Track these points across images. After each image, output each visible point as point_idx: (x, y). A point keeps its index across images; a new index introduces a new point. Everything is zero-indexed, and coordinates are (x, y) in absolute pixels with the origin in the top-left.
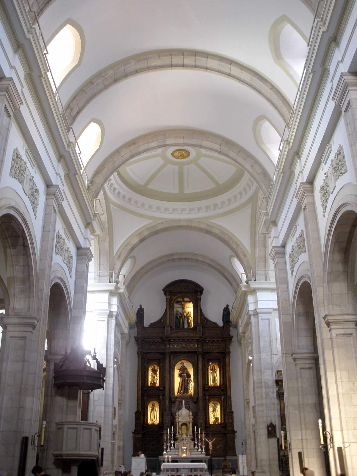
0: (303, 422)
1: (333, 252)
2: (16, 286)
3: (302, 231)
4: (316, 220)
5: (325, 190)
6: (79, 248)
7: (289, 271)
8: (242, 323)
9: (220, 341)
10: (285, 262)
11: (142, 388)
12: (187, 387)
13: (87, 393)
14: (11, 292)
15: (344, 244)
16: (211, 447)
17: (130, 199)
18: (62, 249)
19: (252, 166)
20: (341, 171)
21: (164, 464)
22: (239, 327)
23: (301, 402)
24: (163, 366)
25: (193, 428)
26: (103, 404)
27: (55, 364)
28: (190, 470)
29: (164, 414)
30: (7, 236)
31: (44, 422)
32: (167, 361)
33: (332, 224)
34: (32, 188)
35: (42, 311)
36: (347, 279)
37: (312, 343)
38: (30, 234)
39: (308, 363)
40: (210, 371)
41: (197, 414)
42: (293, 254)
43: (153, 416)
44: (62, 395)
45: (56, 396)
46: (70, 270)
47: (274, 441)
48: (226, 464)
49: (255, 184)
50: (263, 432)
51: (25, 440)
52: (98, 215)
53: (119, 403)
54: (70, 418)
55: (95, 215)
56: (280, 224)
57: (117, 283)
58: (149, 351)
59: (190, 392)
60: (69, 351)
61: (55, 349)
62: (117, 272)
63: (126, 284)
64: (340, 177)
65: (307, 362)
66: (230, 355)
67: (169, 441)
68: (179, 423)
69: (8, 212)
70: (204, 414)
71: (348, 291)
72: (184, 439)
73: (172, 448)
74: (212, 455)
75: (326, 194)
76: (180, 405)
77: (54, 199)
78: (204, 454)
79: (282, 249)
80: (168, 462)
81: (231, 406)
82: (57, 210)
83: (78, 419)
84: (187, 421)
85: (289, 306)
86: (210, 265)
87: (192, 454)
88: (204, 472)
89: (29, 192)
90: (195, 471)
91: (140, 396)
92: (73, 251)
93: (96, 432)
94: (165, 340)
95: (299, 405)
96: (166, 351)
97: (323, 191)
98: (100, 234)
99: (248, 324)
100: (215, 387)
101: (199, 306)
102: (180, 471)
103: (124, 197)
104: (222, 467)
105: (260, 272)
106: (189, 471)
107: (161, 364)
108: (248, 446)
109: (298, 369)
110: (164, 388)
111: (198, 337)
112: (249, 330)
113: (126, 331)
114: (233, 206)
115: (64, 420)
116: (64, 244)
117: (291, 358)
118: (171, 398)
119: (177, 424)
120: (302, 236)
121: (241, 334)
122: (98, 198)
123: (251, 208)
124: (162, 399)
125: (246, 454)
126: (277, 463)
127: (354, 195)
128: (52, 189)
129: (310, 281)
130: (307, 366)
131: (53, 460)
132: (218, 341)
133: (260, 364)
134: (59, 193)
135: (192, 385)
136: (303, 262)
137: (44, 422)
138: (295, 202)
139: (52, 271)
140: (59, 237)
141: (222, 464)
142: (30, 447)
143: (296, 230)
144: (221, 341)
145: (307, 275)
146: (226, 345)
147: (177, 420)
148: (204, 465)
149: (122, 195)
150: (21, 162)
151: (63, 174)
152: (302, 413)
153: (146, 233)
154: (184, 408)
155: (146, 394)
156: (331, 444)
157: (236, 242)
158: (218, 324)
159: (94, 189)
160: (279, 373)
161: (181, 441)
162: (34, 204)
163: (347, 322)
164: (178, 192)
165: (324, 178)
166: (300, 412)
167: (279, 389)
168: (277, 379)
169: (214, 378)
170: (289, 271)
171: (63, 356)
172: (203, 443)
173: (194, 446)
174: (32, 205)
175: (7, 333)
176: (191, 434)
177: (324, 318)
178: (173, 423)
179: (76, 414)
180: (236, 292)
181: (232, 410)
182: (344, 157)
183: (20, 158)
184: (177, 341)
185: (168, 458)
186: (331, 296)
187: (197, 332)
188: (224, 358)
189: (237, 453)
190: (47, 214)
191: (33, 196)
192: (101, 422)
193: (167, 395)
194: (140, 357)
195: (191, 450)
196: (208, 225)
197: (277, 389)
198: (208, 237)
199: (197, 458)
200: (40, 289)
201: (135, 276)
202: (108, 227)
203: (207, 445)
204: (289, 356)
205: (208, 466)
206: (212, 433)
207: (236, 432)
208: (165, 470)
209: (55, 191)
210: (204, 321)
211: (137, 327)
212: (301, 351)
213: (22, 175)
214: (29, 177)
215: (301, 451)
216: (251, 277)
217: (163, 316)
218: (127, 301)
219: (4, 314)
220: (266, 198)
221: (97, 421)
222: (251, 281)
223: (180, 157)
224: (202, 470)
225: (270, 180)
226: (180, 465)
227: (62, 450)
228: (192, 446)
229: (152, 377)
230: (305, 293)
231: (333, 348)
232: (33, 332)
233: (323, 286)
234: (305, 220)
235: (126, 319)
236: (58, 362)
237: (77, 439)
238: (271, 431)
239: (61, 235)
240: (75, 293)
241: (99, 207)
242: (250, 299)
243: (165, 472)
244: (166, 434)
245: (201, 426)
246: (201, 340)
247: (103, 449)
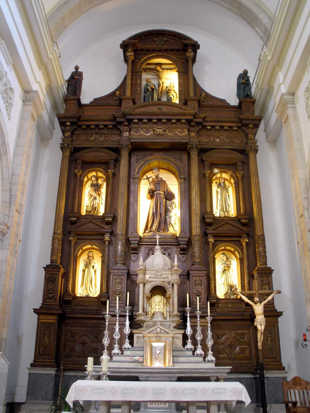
11: (66, 218)
12: (166, 219)
24: (114, 174)
40: (215, 188)
43: (88, 280)
59: (171, 230)
81: (265, 257)
84: (166, 280)
91: (60, 231)
100: (225, 220)
102: (146, 407)
106: (170, 407)
107: (110, 171)
110: (115, 218)
118: (130, 239)
119: (141, 286)
135: (176, 214)
144: (238, 127)
155: (73, 230)
162: (8, 103)
169: (224, 202)
173: (184, 344)
174: (5, 104)
191: (7, 94)
207: (280, 314)
217: (117, 89)
228: (179, 342)
229: (90, 198)
235: (40, 69)
246: (196, 123)
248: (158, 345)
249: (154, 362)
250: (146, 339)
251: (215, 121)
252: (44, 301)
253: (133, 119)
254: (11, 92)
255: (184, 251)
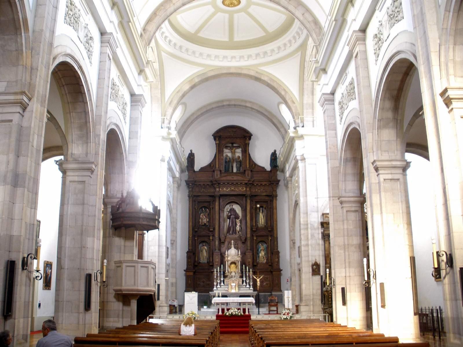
0: (347, 260)
1: (383, 99)
2: (73, 133)
3: (352, 78)
4: (367, 67)
5: (378, 38)
6: (132, 95)
7: (338, 118)
8: (289, 168)
9: (268, 185)
10: (334, 109)
13: (141, 234)
14: (69, 138)
15: (395, 92)
16: (258, 283)
17: (181, 47)
18: (117, 96)
19: (303, 14)
20: (397, 19)
21: (215, 298)
22: (286, 172)
23: (346, 243)
25: (242, 266)
26: (157, 244)
27: (113, 207)
28: (238, 304)
29: (214, 253)
30: (64, 84)
31: (105, 261)
32: (217, 204)
33: (384, 72)
34: (87, 36)
35: (100, 155)
36: (397, 126)
37: (359, 188)
38: (86, 81)
39: (354, 207)
41: (245, 254)
42: (343, 101)
44: (119, 236)
45: (114, 237)
46: (125, 116)
47: (317, 278)
48: (273, 299)
49: (305, 32)
50: (307, 270)
51: (89, 277)
52: (150, 62)
53: (171, 243)
54: (128, 257)
55: (148, 62)
56: (330, 71)
57: (169, 128)
58: (200, 194)
60: (125, 195)
61: (112, 193)
62: (169, 118)
63: (177, 129)
64: (395, 25)
65: (354, 205)
66: (277, 198)
67: (219, 278)
68: (228, 261)
69: (64, 60)
70: (252, 253)
71: (397, 139)
72: (233, 276)
73: (222, 284)
74: (260, 291)
75: (380, 42)
76: (230, 245)
77: (108, 46)
78: (252, 290)
79: (332, 96)
80: (219, 296)
82: (111, 57)
83: (135, 258)
85: (337, 151)
86: (258, 111)
87: (240, 290)
88: (251, 305)
89: (84, 40)
90: (243, 305)
92: (127, 98)
93: (153, 270)
94: (214, 183)
95: (344, 245)
96: (216, 194)
97: (377, 40)
98: (153, 81)
99: (295, 168)
101: (247, 150)
102: (230, 305)
103: (175, 44)
104: (269, 301)
105: (308, 119)
106: (237, 304)
108: (293, 283)
109: (345, 211)
111: (247, 180)
112: (296, 175)
113: (177, 175)
114: (282, 54)
115: (122, 259)
116: (118, 91)
117: (338, 201)
119: (227, 262)
120: (352, 83)
121: (288, 179)
122: (151, 45)
123: (300, 55)
124: (212, 240)
125: (290, 290)
126: (320, 297)
127: (409, 43)
128: (106, 37)
129: (360, 127)
130: (353, 209)
131: (114, 294)
132: (266, 184)
133: (307, 207)
134: (113, 41)
136: (353, 109)
137: (105, 261)
138: (347, 50)
139: (108, 117)
140: (113, 84)
141: (269, 298)
142: (93, 282)
143: (346, 78)
144: (269, 184)
145: (357, 122)
146: (273, 188)
147: (226, 259)
148: (252, 300)
149: (173, 43)
150: (75, 9)
151: (116, 22)
152: (347, 253)
153: (197, 80)
154: (233, 248)
156: (374, 280)
157: (284, 90)
158: (265, 168)
159: (146, 37)
160: (324, 215)
161: (230, 278)
163: (395, 167)
164: (228, 40)
165: (378, 26)
166: (345, 252)
167: (324, 231)
168: (322, 221)
170: (338, 118)
171: (119, 199)
172: (251, 280)
173: (243, 283)
174: (87, 53)
175: (67, 177)
176: (240, 272)
177: (373, 163)
178: (222, 262)
179: (133, 253)
180: (283, 138)
181: (279, 250)
182: (401, 4)
183: (74, 5)
184: (226, 185)
185: (219, 294)
186: (381, 142)
187: (245, 176)
188: (272, 201)
189: (282, 289)
190: (102, 61)
191: (88, 43)
192: (155, 260)
193: (217, 235)
194: (191, 200)
195: (239, 287)
196: (257, 72)
197: (322, 231)
198: (257, 84)
199: (246, 293)
200: (97, 135)
201: (185, 122)
202: (160, 75)
203: (255, 281)
204: (336, 200)
205: (256, 300)
206: (260, 271)
207: (282, 270)
208: (216, 304)
209: (109, 39)
210: (252, 165)
211: (188, 171)
212: (347, 195)
213: (76, 22)
214: (84, 25)
215: (344, 286)
216: (299, 123)
217: (213, 161)
218: (178, 146)
219: (63, 159)
220: (316, 46)
221: (151, 260)
222: (299, 127)
223: (230, 6)
224: (249, 303)
225: (320, 28)
226: (230, 300)
227: (121, 286)
228: (241, 283)
230: (354, 139)
231: (380, 192)
232: (92, 176)
233: (372, 133)
234: (356, 68)
235: (177, 164)
236: (115, 204)
237: (135, 276)
238: (316, 269)
239: (115, 83)
240: (130, 138)
241: (151, 55)
242: (298, 144)
243: (215, 306)
244: (216, 271)
245: (249, 265)
247: (159, 285)
248: (233, 284)
249: (232, 290)
250: (229, 282)
251: (259, 182)
252: (187, 266)
253: (220, 183)
254: (91, 41)
255: (244, 243)
